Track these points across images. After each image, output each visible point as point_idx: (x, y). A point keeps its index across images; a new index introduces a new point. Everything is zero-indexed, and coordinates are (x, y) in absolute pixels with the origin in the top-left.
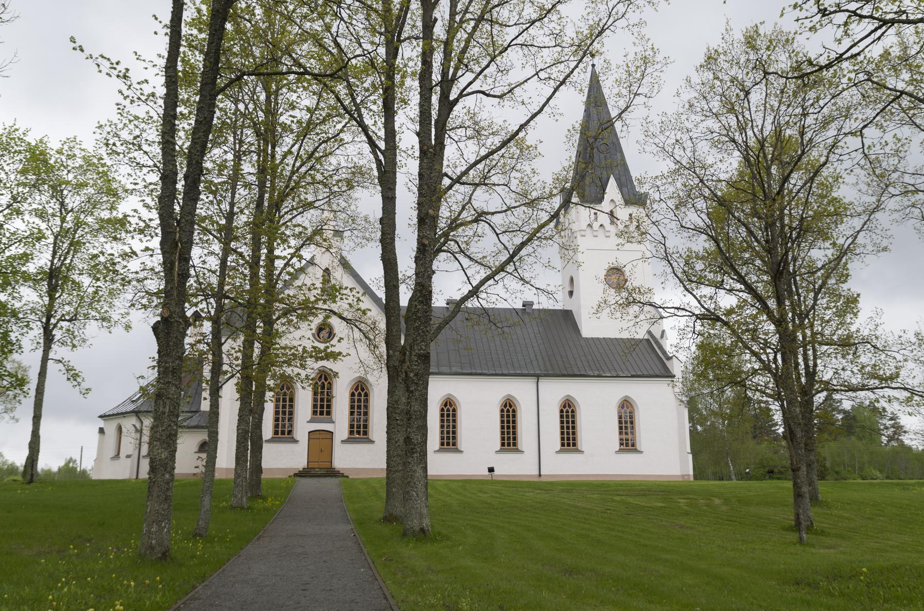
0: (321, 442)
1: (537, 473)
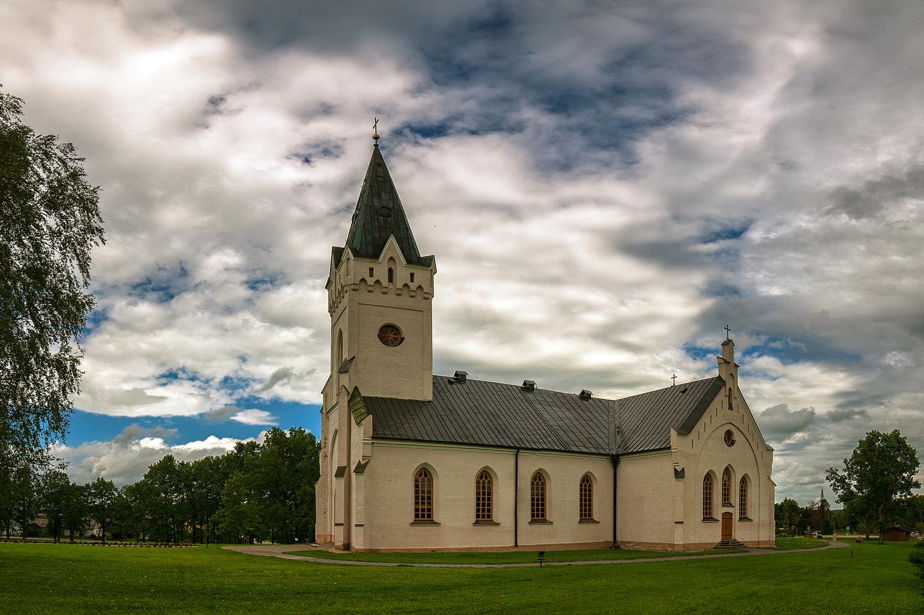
1: (513, 544)
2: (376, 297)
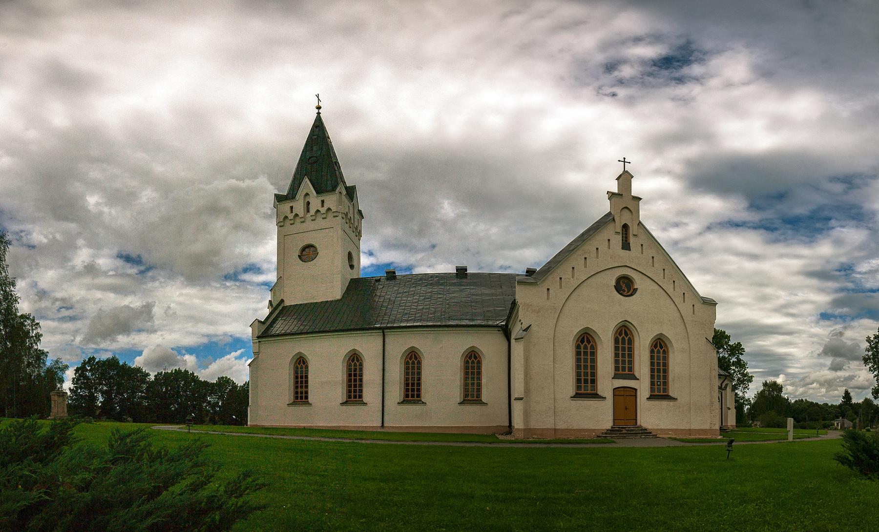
0: (625, 400)
1: (380, 424)
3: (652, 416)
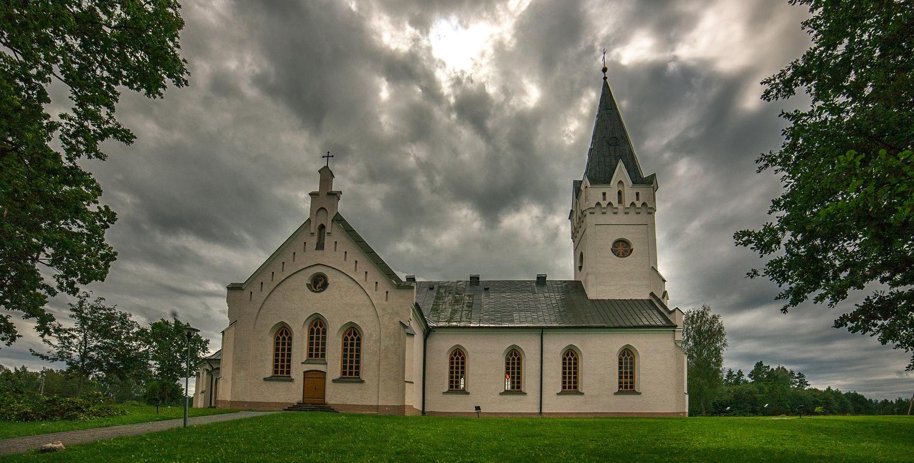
0: (315, 381)
1: (538, 411)
2: (610, 218)
3: (337, 394)
